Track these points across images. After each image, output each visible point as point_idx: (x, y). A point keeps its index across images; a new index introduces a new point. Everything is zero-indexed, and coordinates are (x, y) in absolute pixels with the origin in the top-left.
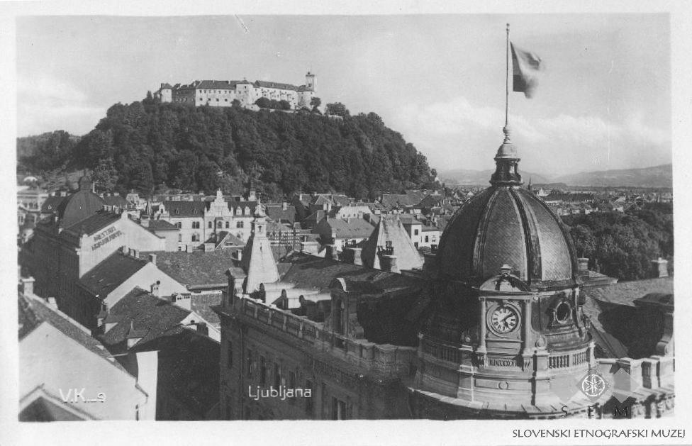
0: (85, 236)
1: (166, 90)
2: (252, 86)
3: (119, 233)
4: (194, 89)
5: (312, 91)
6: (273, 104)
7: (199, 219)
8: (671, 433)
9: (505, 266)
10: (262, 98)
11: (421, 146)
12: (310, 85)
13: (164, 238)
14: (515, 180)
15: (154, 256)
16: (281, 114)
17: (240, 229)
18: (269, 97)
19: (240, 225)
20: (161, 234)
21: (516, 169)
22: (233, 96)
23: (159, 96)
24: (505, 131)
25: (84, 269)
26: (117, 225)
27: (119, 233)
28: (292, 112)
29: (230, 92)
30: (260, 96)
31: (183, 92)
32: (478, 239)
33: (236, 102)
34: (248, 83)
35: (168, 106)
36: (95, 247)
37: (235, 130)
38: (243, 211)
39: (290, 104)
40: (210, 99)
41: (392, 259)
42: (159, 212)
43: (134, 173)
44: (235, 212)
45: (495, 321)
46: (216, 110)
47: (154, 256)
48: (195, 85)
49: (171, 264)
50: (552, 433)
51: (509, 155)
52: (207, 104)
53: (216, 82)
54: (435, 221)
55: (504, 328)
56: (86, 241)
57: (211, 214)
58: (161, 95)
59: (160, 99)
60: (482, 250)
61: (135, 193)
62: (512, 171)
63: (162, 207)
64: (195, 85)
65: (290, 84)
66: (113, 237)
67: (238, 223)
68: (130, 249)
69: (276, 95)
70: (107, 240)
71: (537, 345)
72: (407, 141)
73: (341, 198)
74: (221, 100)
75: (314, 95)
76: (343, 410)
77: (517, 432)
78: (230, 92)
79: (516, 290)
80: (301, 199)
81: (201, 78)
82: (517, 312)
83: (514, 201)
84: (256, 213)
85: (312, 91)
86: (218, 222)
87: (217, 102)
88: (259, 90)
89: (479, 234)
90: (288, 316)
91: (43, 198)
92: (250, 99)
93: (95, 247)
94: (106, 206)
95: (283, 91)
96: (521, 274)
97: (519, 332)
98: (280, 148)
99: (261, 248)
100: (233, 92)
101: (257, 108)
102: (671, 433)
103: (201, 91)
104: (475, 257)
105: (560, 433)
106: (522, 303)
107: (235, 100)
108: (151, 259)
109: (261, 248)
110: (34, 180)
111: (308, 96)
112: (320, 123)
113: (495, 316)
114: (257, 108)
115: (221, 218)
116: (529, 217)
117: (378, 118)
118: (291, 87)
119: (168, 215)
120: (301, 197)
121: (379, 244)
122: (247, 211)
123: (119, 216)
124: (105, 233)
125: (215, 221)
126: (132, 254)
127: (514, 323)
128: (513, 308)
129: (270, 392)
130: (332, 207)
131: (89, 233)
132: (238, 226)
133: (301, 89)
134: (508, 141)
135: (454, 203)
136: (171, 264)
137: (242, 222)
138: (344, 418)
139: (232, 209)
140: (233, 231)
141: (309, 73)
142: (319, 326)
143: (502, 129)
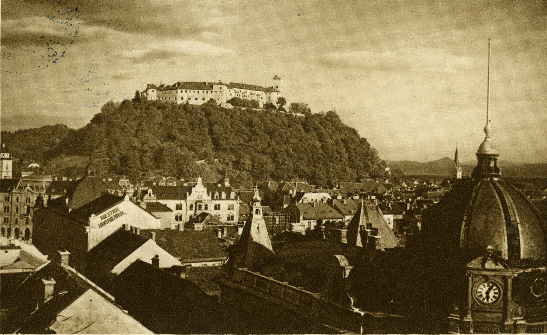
0: (93, 215)
2: (226, 87)
3: (122, 213)
5: (278, 92)
6: (245, 103)
7: (183, 202)
9: (489, 247)
10: (235, 98)
11: (373, 143)
12: (277, 87)
13: (160, 218)
14: (495, 172)
15: (154, 234)
16: (250, 111)
17: (217, 211)
18: (242, 98)
19: (217, 207)
20: (157, 214)
21: (495, 163)
23: (145, 94)
24: (485, 130)
25: (92, 245)
26: (121, 206)
27: (122, 213)
28: (261, 110)
30: (234, 95)
32: (464, 223)
34: (222, 84)
35: (154, 103)
36: (101, 225)
37: (211, 125)
38: (220, 196)
39: (259, 103)
40: (189, 99)
41: (376, 239)
42: (147, 196)
43: (124, 160)
44: (213, 195)
45: (479, 294)
46: (194, 107)
47: (154, 234)
48: (177, 86)
49: (166, 239)
51: (489, 150)
52: (187, 103)
53: (250, 86)
54: (390, 206)
55: (484, 299)
56: (94, 220)
57: (192, 198)
58: (147, 94)
59: (146, 98)
60: (467, 231)
61: (127, 178)
62: (492, 164)
63: (150, 191)
64: (177, 86)
65: (259, 85)
66: (117, 216)
67: (177, 205)
68: (131, 227)
69: (248, 95)
70: (112, 220)
71: (517, 315)
72: (362, 136)
73: (304, 185)
74: (197, 98)
75: (280, 95)
78: (207, 92)
79: (500, 267)
80: (269, 185)
81: (181, 80)
82: (500, 287)
83: (494, 190)
84: (254, 198)
85: (278, 92)
86: (198, 204)
87: (196, 101)
88: (232, 91)
89: (465, 218)
90: (285, 286)
91: (47, 182)
92: (223, 97)
93: (101, 225)
94: (109, 190)
95: (253, 92)
96: (503, 254)
97: (502, 305)
98: (249, 141)
99: (258, 228)
100: (209, 92)
101: (230, 106)
103: (182, 92)
104: (461, 238)
106: (504, 278)
107: (211, 99)
108: (151, 236)
109: (258, 228)
110: (37, 167)
111: (275, 97)
112: (285, 120)
113: (479, 290)
114: (230, 106)
115: (201, 201)
116: (509, 205)
117: (336, 116)
118: (259, 89)
119: (155, 198)
120: (269, 183)
121: (360, 223)
122: (224, 195)
123: (122, 199)
124: (110, 213)
125: (196, 203)
126: (134, 232)
127: (497, 296)
128: (496, 283)
130: (297, 193)
131: (97, 213)
132: (215, 209)
133: (270, 90)
134: (488, 139)
135: (403, 190)
136: (166, 239)
137: (219, 205)
139: (211, 193)
140: (211, 211)
141: (276, 76)
142: (316, 296)
143: (483, 128)
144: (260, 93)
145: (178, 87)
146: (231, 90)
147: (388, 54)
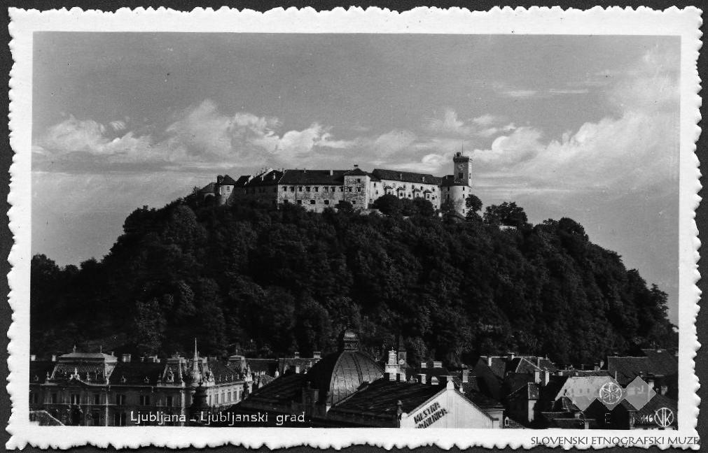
1: (226, 187)
2: (368, 178)
4: (276, 183)
22: (338, 196)
27: (444, 412)
29: (308, 189)
33: (343, 205)
34: (364, 174)
74: (316, 201)
76: (34, 386)
95: (418, 186)
100: (337, 188)
102: (687, 440)
105: (577, 440)
117: (579, 229)
118: (429, 179)
124: (427, 412)
129: (284, 419)
133: (446, 183)
138: (30, 386)
144: (429, 187)
145: (277, 180)
146: (378, 184)
147: (148, 179)
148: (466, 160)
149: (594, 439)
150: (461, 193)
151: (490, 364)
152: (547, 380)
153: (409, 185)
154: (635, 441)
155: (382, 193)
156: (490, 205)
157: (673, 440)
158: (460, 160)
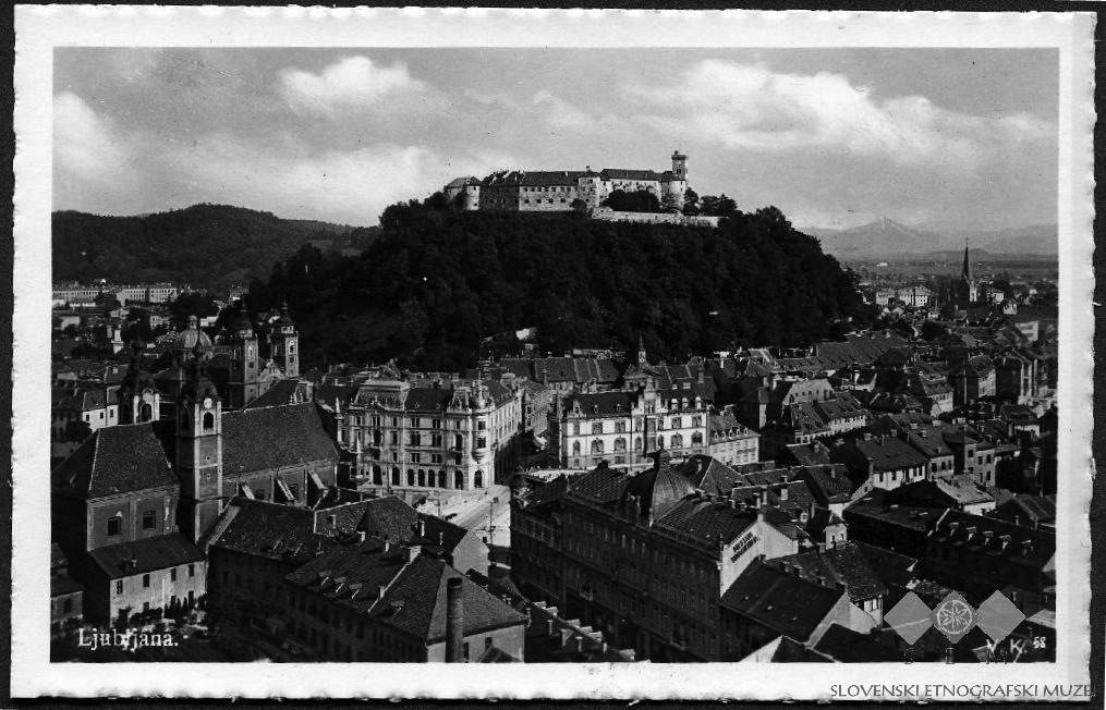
2: (599, 179)
4: (518, 186)
8: (1074, 689)
22: (573, 195)
26: (753, 530)
29: (569, 189)
31: (502, 186)
33: (577, 203)
36: (734, 559)
50: (891, 690)
56: (728, 552)
70: (745, 549)
74: (555, 203)
77: (837, 689)
100: (572, 188)
102: (1074, 689)
105: (903, 689)
118: (650, 175)
133: (667, 178)
148: (683, 158)
149: (929, 688)
150: (678, 188)
151: (722, 367)
152: (775, 385)
153: (634, 182)
154: (992, 692)
155: (610, 190)
156: (687, 164)
157: (1051, 689)
158: (678, 158)
